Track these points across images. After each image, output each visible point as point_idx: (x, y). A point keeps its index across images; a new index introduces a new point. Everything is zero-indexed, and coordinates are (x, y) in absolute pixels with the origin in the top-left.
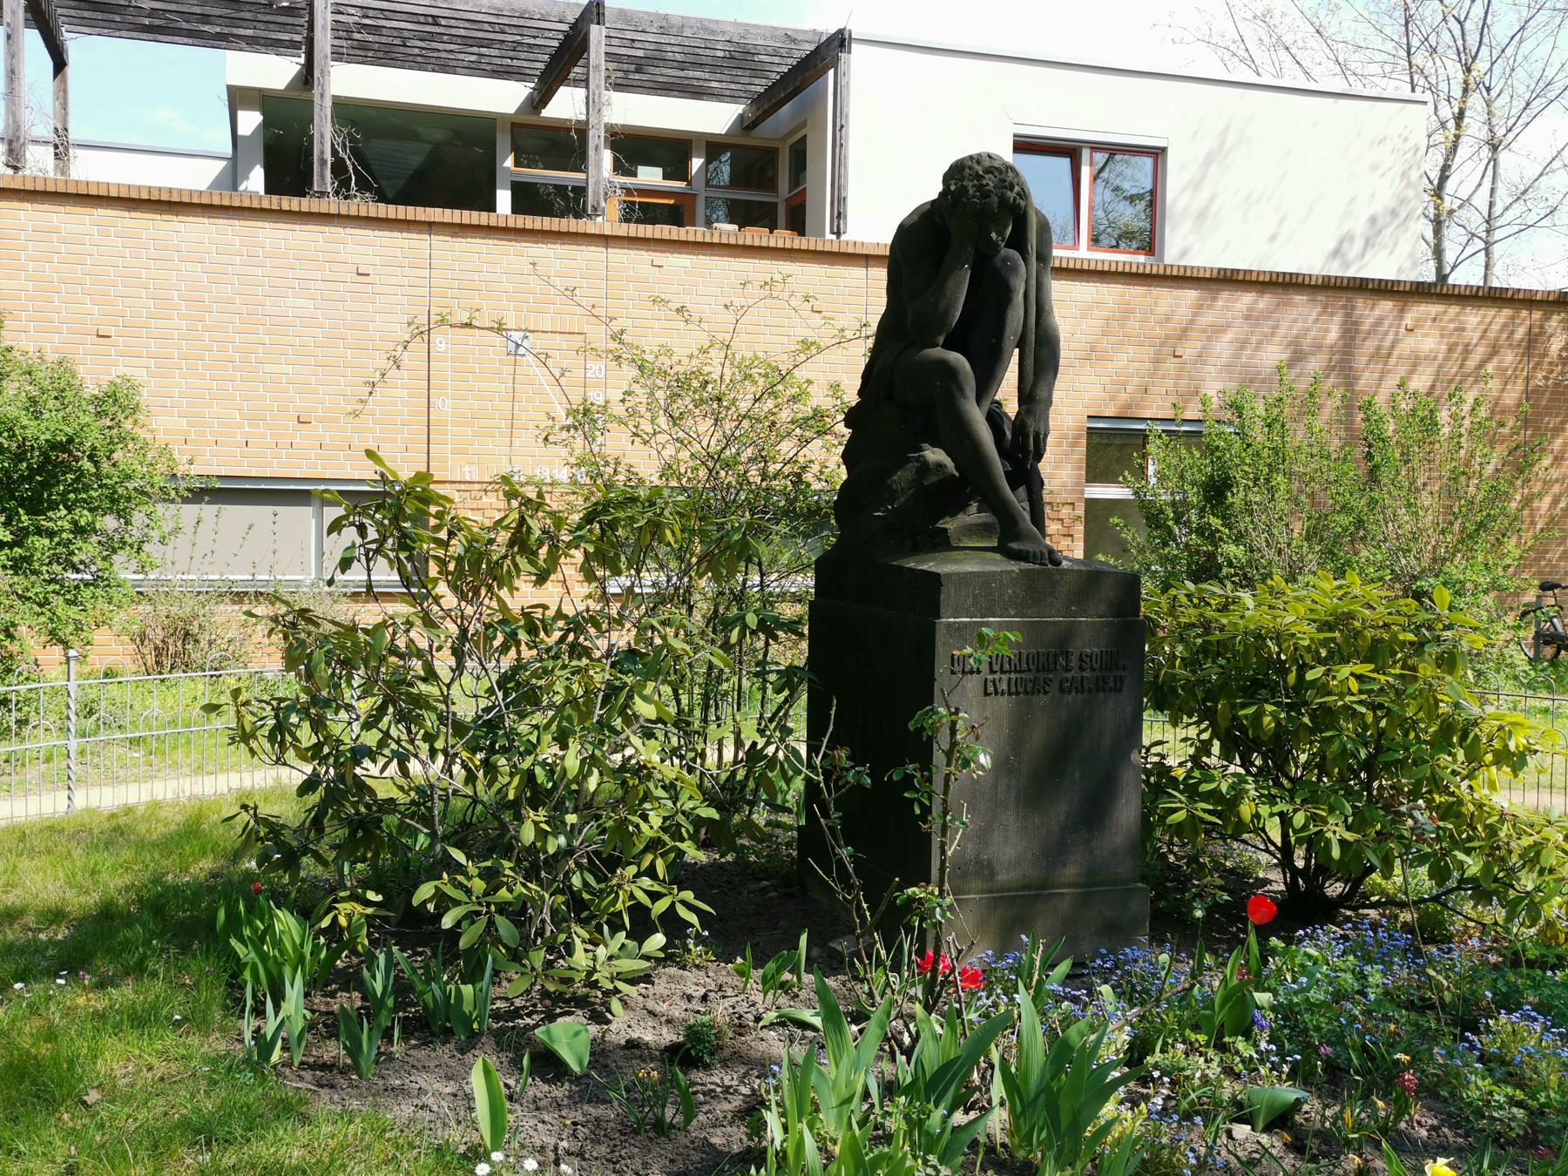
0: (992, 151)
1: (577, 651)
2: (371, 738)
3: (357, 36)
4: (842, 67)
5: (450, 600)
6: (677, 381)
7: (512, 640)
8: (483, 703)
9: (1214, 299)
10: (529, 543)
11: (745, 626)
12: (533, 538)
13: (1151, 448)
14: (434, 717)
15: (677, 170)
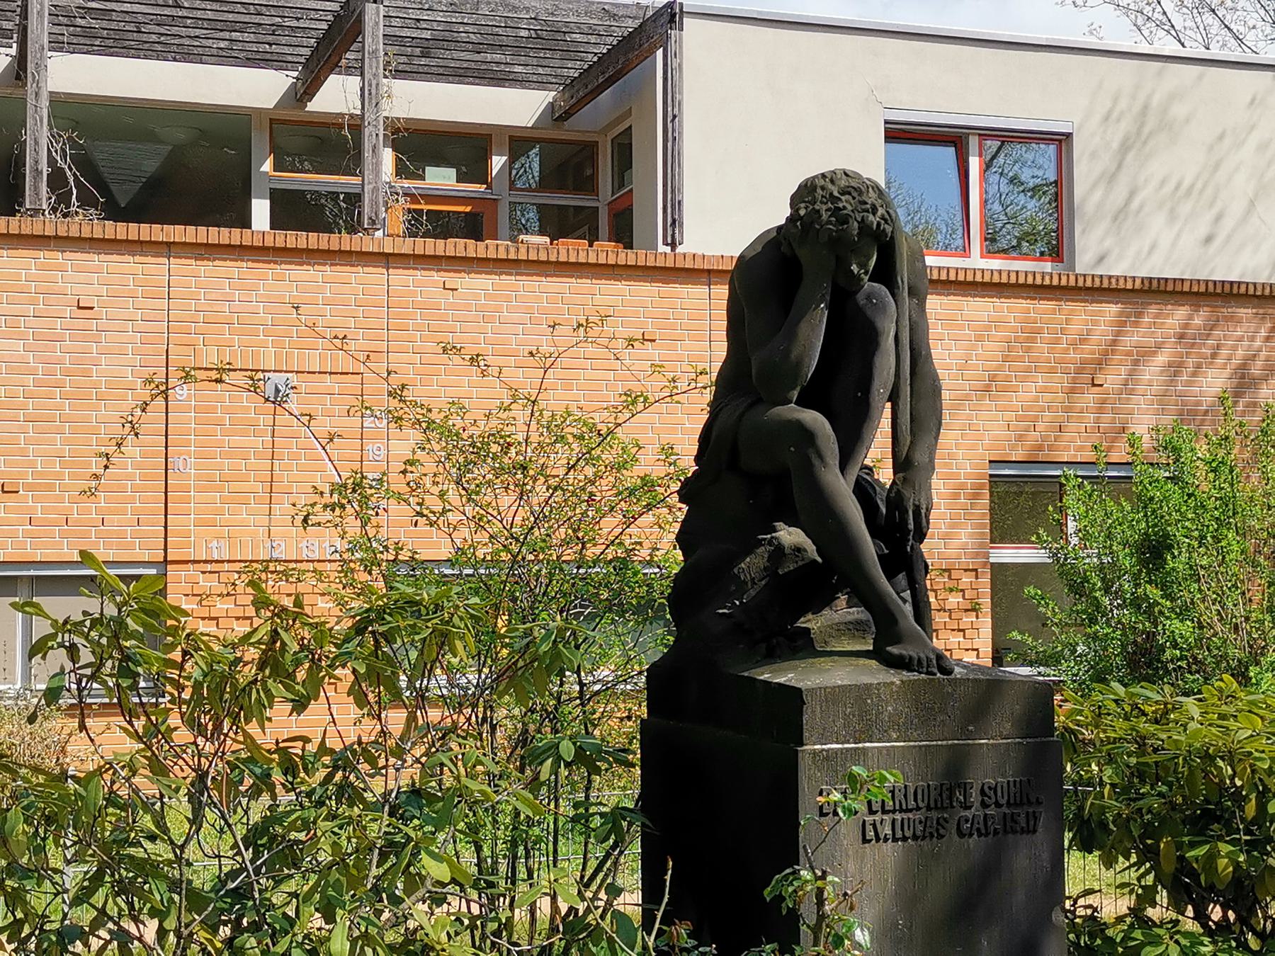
0: (850, 167)
1: (348, 793)
2: (84, 916)
3: (80, 21)
4: (672, 46)
5: (183, 735)
6: (473, 445)
7: (264, 783)
8: (228, 865)
9: (1139, 315)
10: (286, 663)
11: (559, 758)
12: (288, 657)
13: (1069, 500)
14: (163, 887)
15: (474, 169)
